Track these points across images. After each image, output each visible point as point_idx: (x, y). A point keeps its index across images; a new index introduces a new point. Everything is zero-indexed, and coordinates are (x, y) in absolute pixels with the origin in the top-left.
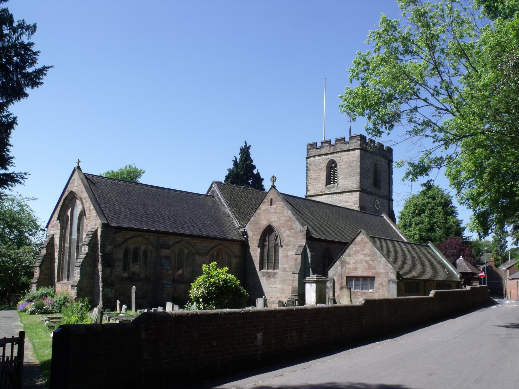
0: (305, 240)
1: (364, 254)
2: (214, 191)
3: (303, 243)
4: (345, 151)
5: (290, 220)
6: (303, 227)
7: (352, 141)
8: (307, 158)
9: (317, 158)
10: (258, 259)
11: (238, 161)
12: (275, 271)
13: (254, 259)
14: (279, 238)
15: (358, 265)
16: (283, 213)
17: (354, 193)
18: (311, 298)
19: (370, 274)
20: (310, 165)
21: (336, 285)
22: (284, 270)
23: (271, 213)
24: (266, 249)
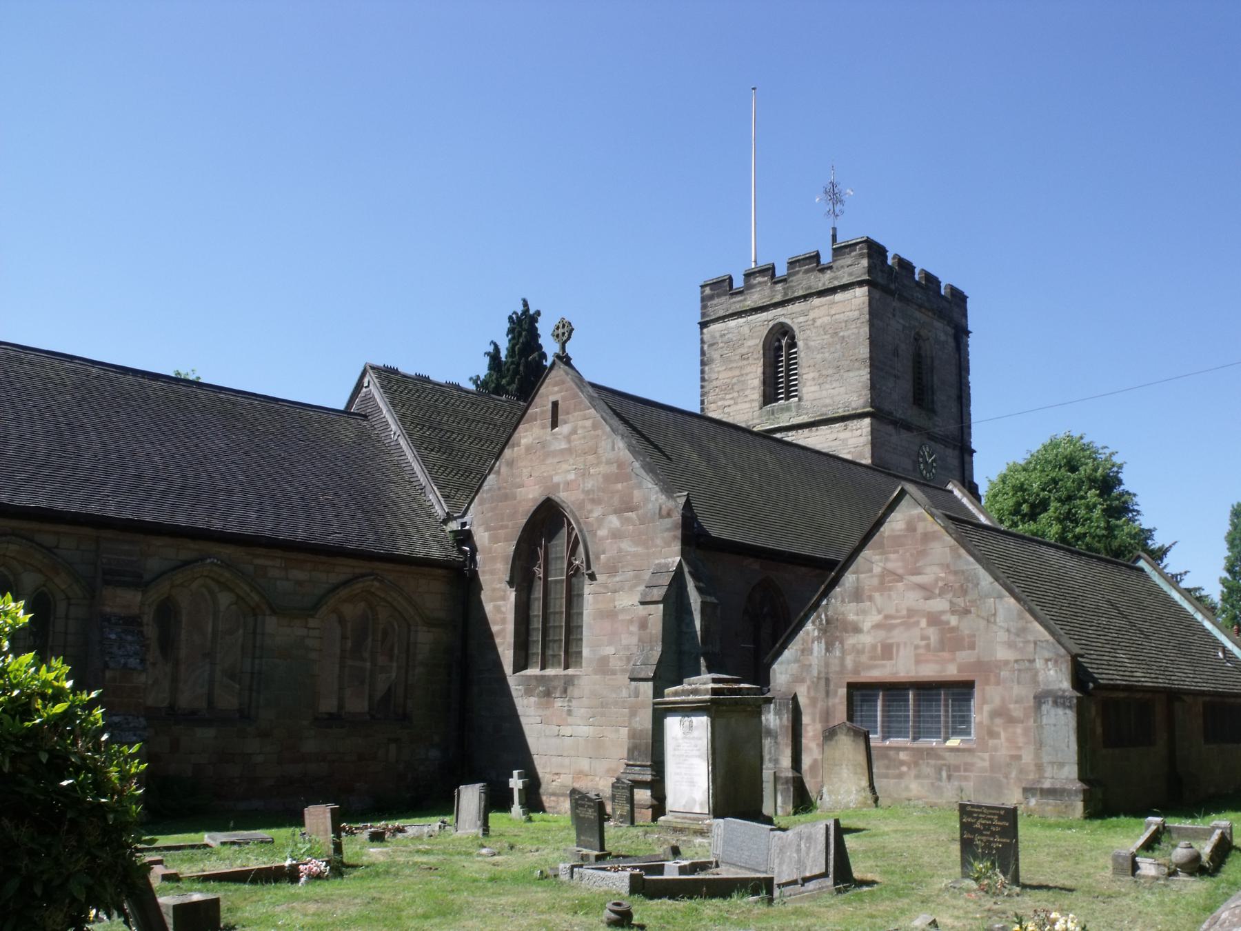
0: (677, 547)
1: (922, 587)
2: (369, 398)
3: (672, 558)
4: (821, 294)
5: (621, 475)
6: (674, 499)
7: (840, 262)
8: (703, 325)
9: (732, 323)
10: (510, 627)
11: (503, 354)
12: (570, 671)
13: (495, 629)
14: (581, 548)
15: (898, 636)
18: (692, 783)
19: (951, 672)
20: (711, 345)
21: (806, 719)
22: (603, 666)
23: (554, 454)
24: (538, 593)
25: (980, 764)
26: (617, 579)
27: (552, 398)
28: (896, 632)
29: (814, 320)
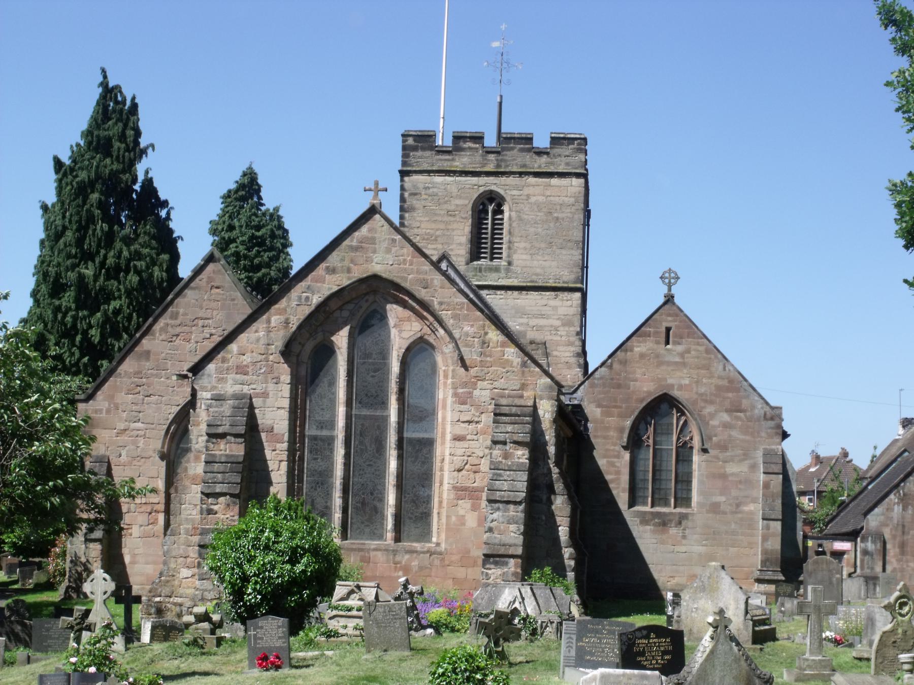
7: (557, 151)
9: (439, 179)
16: (707, 367)
17: (566, 295)
21: (888, 546)
26: (728, 454)
27: (665, 325)
29: (528, 196)
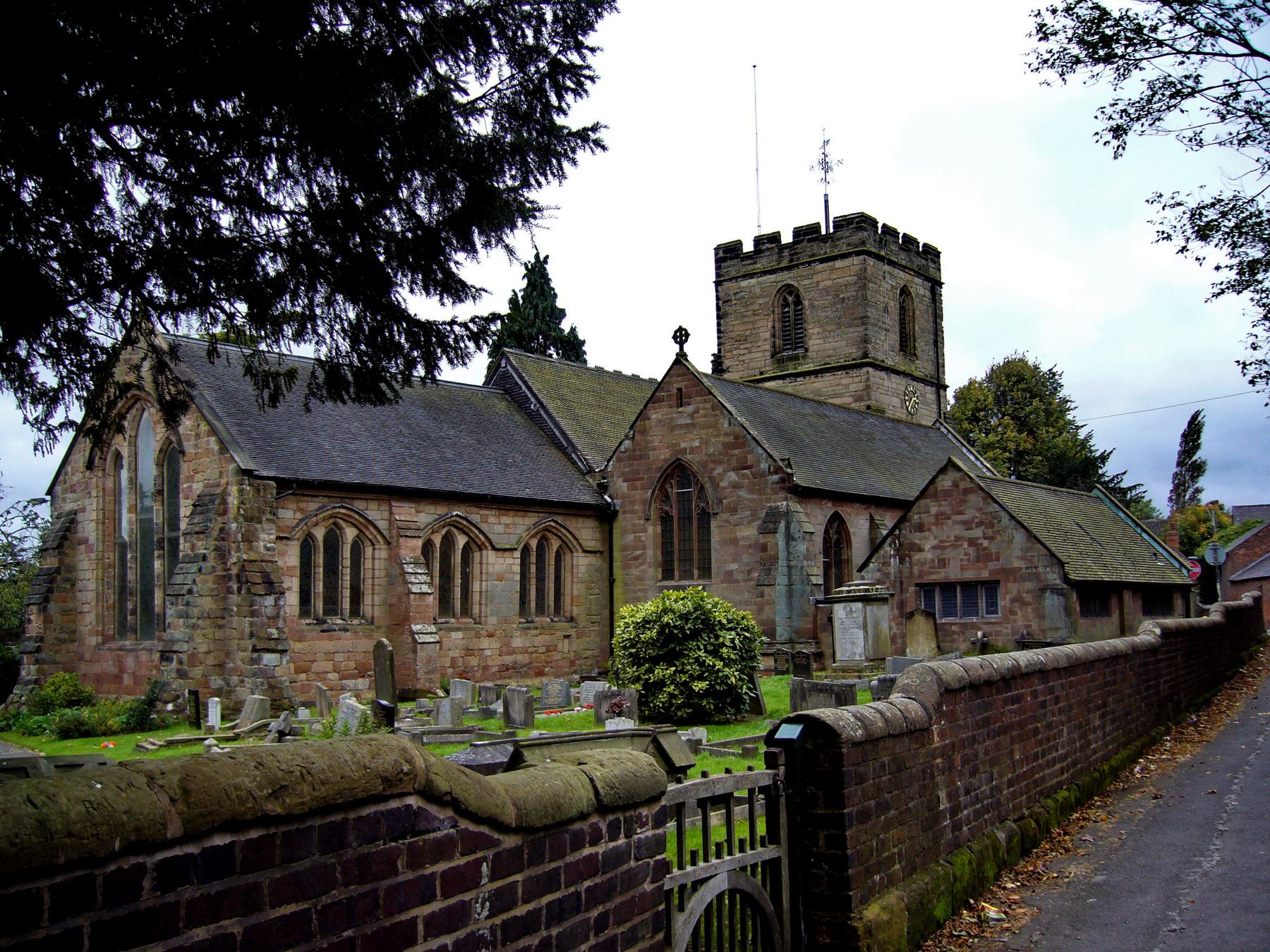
4: (822, 261)
15: (948, 554)
16: (714, 426)
19: (985, 575)
25: (1005, 631)
28: (947, 551)
29: (818, 284)
